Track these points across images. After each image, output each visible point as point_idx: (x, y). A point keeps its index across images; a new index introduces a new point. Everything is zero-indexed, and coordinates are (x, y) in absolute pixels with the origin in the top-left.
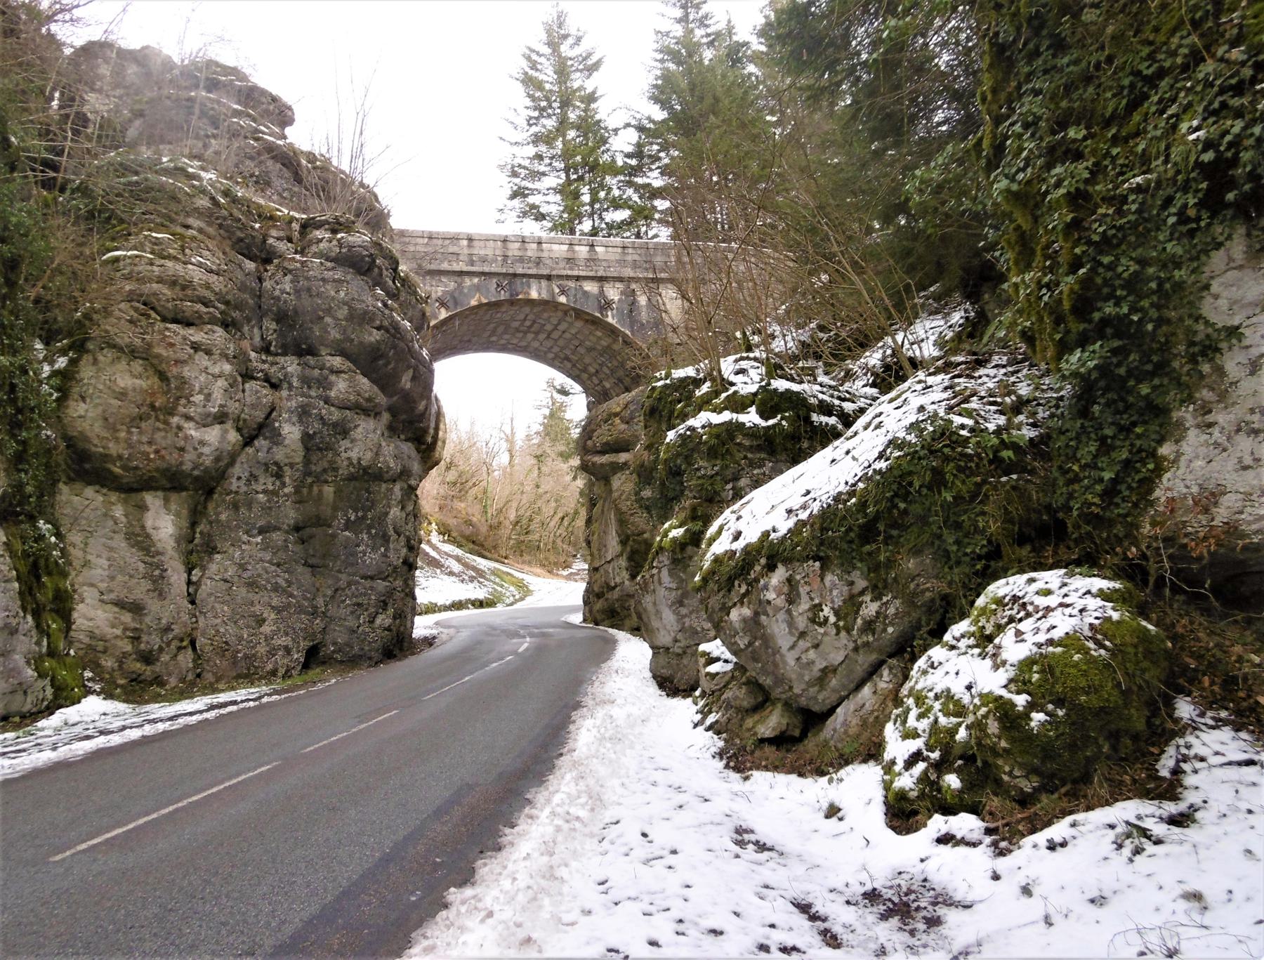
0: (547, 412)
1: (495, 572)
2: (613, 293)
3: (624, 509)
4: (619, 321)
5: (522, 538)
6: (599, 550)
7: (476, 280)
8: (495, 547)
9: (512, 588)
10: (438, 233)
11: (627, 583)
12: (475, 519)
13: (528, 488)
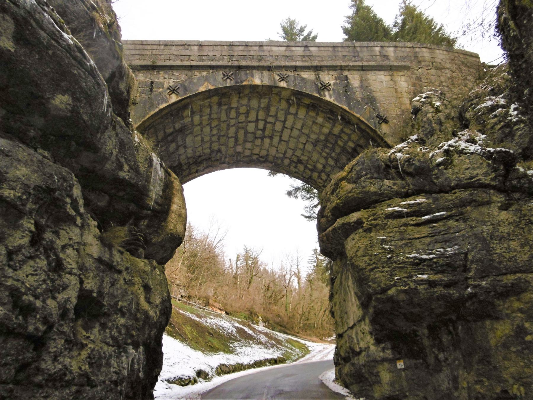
0: (315, 264)
1: (288, 341)
2: (328, 78)
3: (362, 265)
4: (336, 99)
5: (305, 322)
6: (342, 318)
7: (205, 73)
8: (292, 328)
9: (297, 350)
10: (173, 42)
11: (372, 348)
12: (281, 314)
13: (307, 295)
